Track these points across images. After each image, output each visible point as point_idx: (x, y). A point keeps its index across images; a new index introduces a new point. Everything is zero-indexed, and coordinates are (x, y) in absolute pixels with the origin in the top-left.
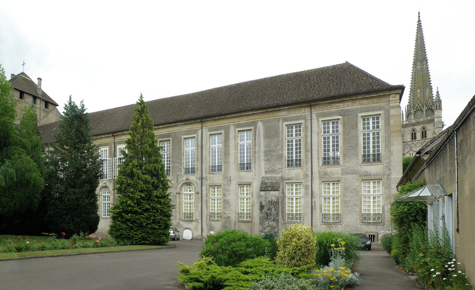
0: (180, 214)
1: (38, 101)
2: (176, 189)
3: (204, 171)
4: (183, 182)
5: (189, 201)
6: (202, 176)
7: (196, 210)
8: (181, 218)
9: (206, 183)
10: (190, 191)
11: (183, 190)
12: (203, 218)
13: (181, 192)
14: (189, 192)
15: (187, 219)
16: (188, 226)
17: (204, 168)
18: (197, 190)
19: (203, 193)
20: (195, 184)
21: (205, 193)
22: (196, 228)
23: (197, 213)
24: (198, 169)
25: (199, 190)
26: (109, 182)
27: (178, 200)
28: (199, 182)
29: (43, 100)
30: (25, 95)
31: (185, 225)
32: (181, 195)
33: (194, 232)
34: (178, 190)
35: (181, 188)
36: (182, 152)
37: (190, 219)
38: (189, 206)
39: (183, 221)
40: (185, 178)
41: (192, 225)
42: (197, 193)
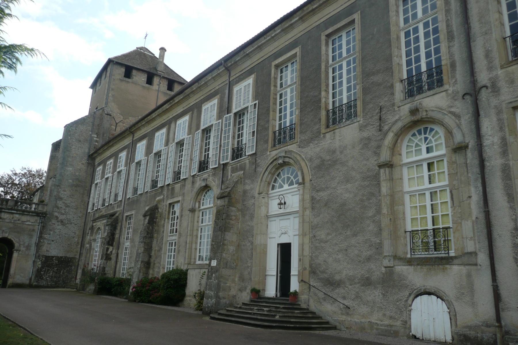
0: (395, 236)
1: (156, 80)
2: (377, 154)
3: (480, 62)
4: (400, 125)
5: (427, 185)
6: (474, 82)
7: (460, 216)
8: (400, 254)
9: (494, 102)
10: (428, 150)
11: (404, 151)
12: (497, 232)
13: (395, 160)
14: (424, 155)
15: (423, 255)
16: (431, 283)
17: (479, 54)
18: (458, 138)
19: (487, 142)
20: (449, 121)
21: (496, 139)
22: (468, 289)
23: (467, 226)
24: (453, 65)
25: (463, 134)
26: (214, 175)
27: (384, 189)
28: (463, 108)
29: (164, 78)
30: (134, 72)
31: (416, 277)
32: (396, 171)
33: (460, 308)
34: (385, 156)
35: (394, 148)
36: (393, 36)
37: (435, 254)
38: (428, 203)
39: (410, 262)
40: (406, 109)
41: (448, 280)
42: (460, 149)
